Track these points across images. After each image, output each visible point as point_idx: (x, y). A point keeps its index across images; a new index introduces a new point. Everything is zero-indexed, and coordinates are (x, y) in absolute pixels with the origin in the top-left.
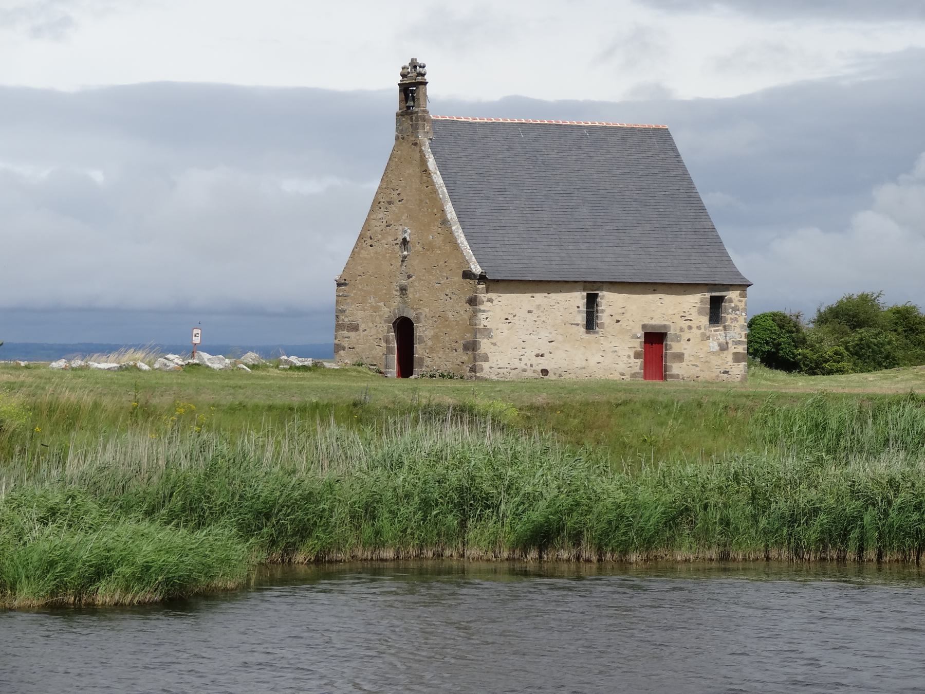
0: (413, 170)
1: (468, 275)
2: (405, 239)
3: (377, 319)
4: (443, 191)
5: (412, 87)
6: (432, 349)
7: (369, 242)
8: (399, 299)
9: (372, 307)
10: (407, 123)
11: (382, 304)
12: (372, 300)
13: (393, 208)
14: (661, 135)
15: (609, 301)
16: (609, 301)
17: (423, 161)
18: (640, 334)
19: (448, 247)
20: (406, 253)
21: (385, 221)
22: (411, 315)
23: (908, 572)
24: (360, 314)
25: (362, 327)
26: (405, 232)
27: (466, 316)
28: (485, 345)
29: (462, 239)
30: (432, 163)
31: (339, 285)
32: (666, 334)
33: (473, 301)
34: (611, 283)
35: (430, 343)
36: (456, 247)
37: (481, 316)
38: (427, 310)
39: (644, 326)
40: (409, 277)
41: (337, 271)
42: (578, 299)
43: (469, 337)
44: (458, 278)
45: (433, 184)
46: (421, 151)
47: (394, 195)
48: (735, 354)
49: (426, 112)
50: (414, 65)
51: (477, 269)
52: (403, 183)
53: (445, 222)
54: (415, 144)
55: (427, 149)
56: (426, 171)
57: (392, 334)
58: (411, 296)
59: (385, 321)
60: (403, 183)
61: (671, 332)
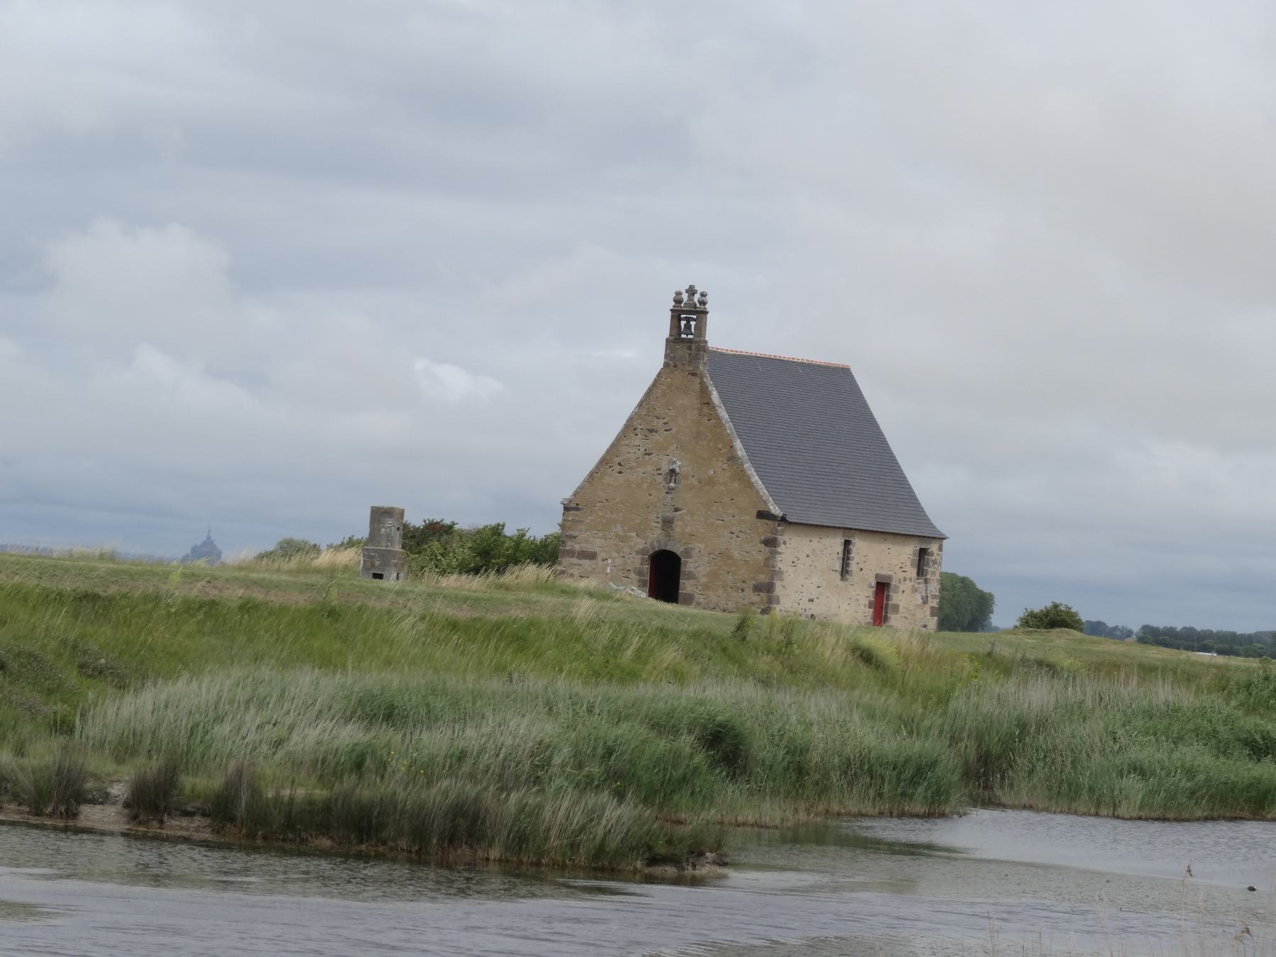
0: (689, 401)
1: (764, 515)
2: (673, 471)
3: (627, 550)
4: (729, 426)
5: (688, 314)
6: (706, 587)
7: (618, 468)
8: (659, 531)
9: (617, 536)
10: (682, 351)
11: (634, 534)
12: (619, 529)
13: (656, 437)
14: (837, 383)
15: (860, 546)
16: (860, 546)
17: (704, 392)
18: (874, 584)
19: (736, 485)
20: (672, 485)
21: (642, 450)
22: (678, 549)
23: (104, 619)
24: (599, 542)
25: (602, 555)
26: (674, 463)
27: (760, 558)
28: (778, 590)
29: (755, 478)
30: (715, 397)
31: (567, 509)
32: (888, 585)
33: (771, 543)
34: (861, 530)
35: (704, 580)
36: (750, 485)
37: (779, 558)
38: (702, 546)
39: (877, 576)
40: (677, 510)
41: (568, 494)
42: (836, 543)
43: (762, 578)
44: (750, 517)
45: (718, 418)
46: (702, 383)
47: (659, 424)
48: (932, 608)
49: (706, 342)
50: (692, 291)
51: (775, 510)
52: (673, 413)
53: (732, 458)
54: (694, 374)
55: (708, 380)
56: (709, 403)
57: (647, 567)
58: (678, 530)
59: (637, 553)
60: (673, 413)
61: (893, 583)
